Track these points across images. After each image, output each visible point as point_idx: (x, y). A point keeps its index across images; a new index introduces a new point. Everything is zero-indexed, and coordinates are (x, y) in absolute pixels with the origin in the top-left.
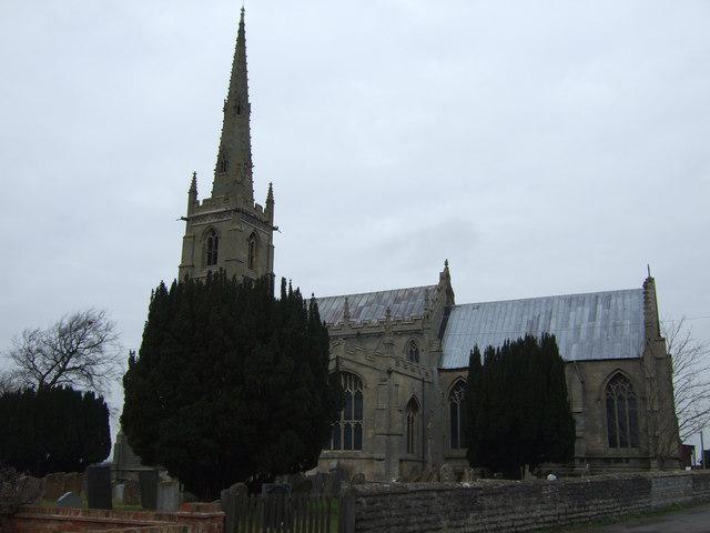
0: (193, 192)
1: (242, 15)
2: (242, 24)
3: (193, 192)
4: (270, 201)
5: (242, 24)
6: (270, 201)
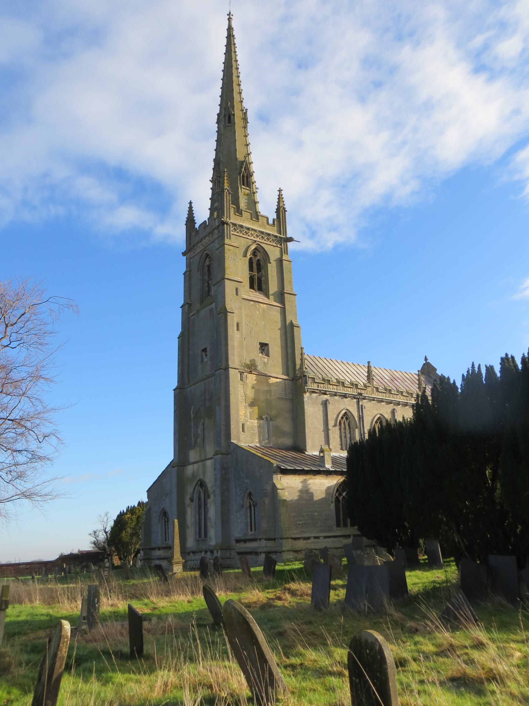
0: (190, 220)
1: (229, 19)
2: (230, 29)
3: (190, 220)
4: (281, 211)
5: (230, 29)
6: (281, 211)
